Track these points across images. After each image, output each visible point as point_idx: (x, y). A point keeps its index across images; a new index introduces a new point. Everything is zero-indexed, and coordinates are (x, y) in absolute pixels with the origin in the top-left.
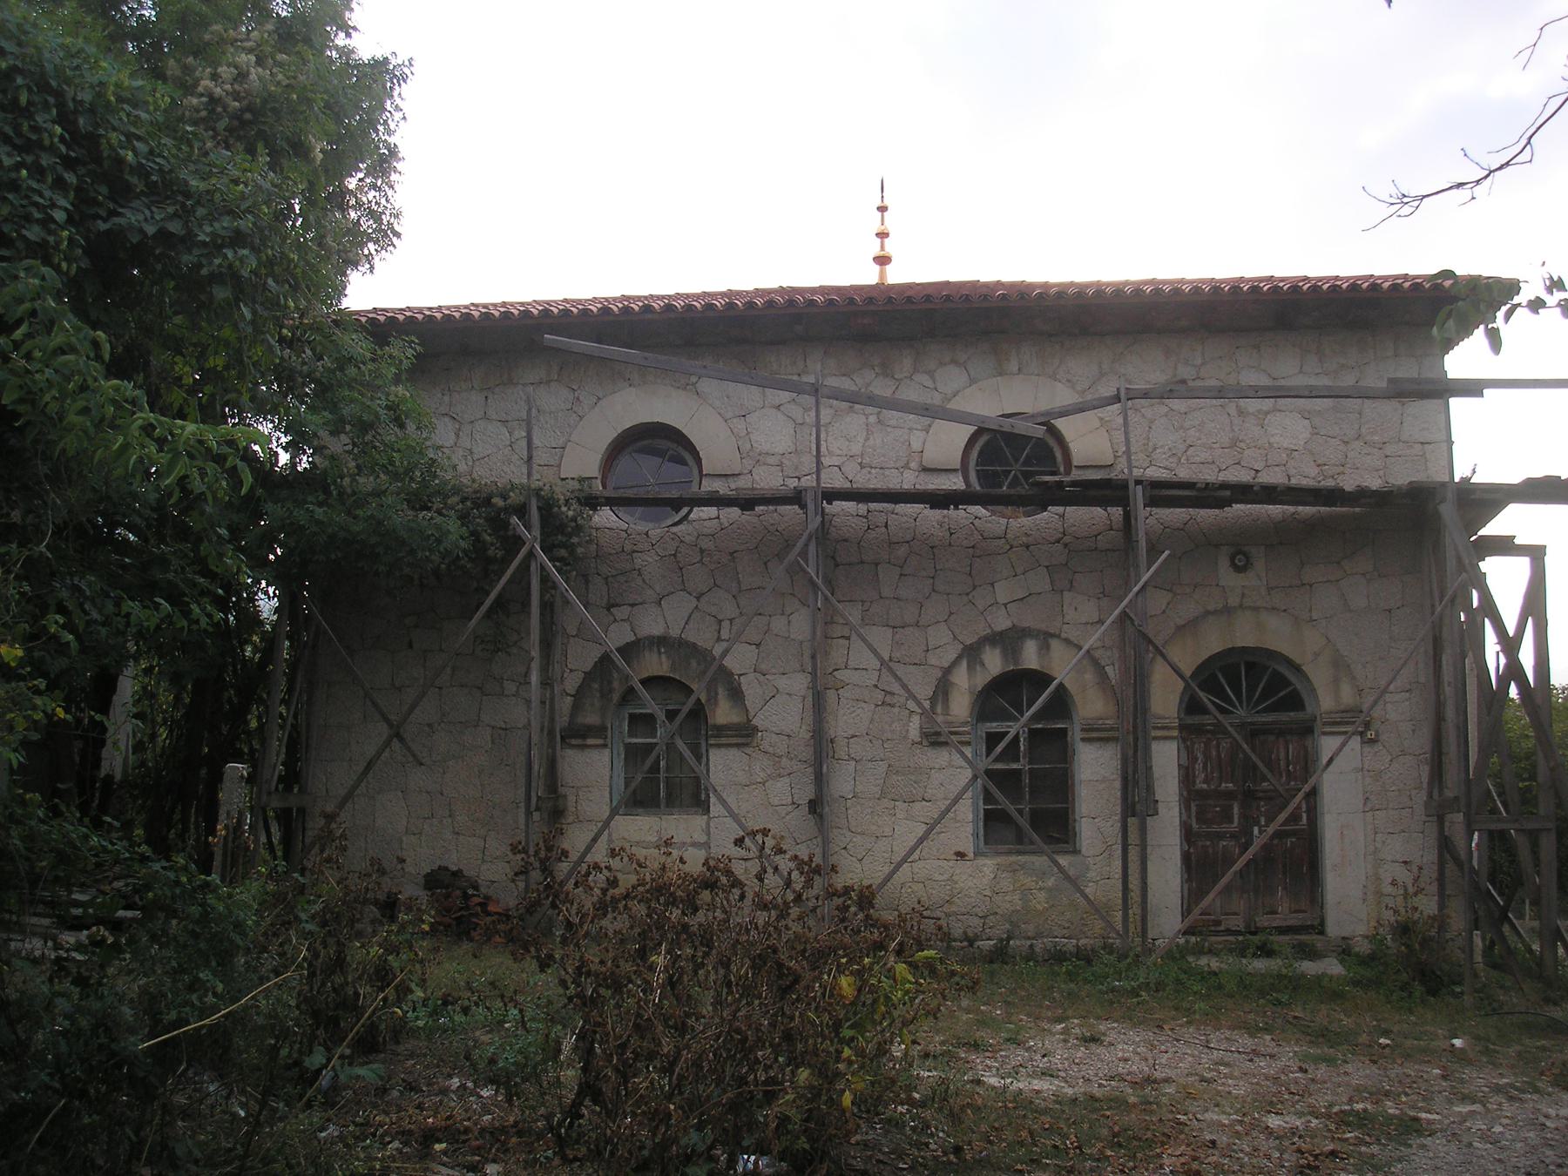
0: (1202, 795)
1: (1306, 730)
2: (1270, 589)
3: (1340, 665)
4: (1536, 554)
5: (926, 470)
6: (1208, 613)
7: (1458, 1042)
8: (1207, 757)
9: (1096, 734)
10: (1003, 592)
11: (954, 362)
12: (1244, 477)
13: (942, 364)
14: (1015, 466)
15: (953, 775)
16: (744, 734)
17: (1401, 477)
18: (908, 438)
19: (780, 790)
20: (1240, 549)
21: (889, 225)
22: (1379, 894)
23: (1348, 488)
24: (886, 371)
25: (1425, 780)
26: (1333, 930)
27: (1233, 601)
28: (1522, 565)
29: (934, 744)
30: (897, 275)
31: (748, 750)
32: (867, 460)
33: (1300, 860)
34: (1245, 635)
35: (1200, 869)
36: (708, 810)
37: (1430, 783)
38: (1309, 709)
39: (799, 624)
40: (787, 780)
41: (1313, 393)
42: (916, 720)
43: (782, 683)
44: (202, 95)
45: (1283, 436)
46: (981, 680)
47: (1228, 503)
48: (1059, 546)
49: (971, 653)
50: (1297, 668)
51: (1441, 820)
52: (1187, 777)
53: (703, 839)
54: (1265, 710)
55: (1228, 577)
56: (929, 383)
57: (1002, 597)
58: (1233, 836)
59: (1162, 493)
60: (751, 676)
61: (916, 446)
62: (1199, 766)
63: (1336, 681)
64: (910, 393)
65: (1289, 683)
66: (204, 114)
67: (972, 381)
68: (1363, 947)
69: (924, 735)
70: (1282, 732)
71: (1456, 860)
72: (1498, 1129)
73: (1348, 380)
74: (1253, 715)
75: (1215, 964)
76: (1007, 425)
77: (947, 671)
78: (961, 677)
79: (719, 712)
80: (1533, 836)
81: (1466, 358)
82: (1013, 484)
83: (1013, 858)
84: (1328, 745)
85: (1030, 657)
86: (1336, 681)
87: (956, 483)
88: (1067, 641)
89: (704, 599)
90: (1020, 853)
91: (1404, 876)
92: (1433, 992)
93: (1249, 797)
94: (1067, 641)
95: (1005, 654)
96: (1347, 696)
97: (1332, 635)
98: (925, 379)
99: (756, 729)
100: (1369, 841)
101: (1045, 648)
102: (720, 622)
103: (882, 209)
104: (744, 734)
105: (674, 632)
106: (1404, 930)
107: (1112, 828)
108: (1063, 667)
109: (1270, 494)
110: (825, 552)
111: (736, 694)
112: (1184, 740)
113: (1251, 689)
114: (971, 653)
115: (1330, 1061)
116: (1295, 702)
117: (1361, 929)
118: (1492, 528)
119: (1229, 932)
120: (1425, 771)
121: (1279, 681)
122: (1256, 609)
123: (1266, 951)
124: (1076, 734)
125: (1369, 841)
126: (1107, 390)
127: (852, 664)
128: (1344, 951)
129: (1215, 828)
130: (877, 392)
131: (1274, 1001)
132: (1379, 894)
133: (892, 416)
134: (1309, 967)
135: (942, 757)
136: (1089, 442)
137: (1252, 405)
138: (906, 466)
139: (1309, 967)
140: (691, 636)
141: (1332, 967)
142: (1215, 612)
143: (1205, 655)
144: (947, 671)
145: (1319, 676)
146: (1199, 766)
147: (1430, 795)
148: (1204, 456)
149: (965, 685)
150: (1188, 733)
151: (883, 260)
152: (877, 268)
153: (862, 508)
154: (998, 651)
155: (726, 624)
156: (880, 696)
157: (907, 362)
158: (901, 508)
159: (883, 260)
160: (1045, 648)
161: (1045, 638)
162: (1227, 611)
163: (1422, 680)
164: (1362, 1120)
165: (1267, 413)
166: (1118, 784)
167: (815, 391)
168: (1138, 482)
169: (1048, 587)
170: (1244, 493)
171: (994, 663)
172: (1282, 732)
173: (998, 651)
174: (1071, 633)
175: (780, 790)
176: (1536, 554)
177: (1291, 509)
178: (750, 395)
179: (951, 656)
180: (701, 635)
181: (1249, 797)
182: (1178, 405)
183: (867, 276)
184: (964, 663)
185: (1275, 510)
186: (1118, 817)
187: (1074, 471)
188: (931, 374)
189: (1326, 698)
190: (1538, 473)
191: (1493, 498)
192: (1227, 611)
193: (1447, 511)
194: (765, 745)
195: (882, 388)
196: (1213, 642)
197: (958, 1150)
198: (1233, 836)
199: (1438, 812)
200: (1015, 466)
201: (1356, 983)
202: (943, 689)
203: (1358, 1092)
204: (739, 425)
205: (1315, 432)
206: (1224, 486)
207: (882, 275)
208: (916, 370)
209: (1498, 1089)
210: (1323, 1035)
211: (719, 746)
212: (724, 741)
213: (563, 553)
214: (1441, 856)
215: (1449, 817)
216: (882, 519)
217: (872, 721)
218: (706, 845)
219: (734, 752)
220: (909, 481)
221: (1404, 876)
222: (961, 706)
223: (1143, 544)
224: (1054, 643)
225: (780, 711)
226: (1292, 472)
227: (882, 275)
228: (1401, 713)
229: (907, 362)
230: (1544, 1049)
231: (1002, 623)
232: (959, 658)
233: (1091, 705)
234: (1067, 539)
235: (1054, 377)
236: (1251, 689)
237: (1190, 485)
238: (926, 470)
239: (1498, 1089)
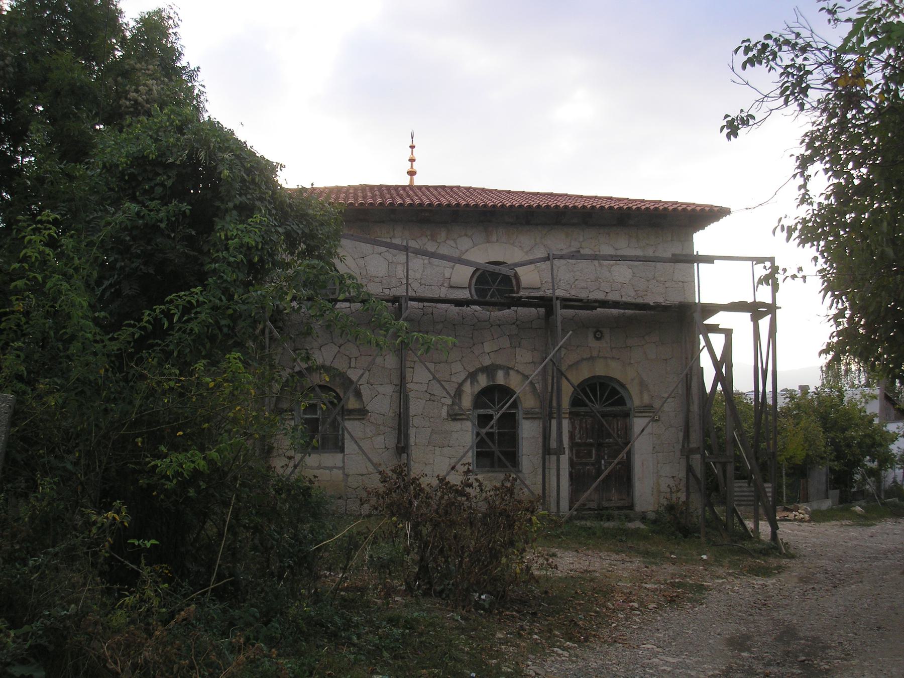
0: (578, 445)
1: (627, 415)
2: (612, 349)
3: (642, 385)
4: (728, 333)
5: (451, 287)
6: (583, 359)
7: (704, 557)
8: (581, 427)
9: (530, 415)
10: (487, 347)
11: (466, 235)
12: (600, 296)
13: (460, 236)
14: (495, 286)
15: (465, 435)
16: (362, 413)
17: (674, 298)
18: (443, 270)
19: (379, 441)
20: (598, 330)
21: (416, 155)
22: (659, 492)
23: (652, 304)
24: (433, 238)
25: (681, 439)
26: (638, 508)
27: (595, 354)
28: (723, 336)
29: (454, 420)
30: (418, 181)
31: (364, 422)
32: (423, 282)
33: (623, 477)
34: (600, 370)
35: (578, 480)
36: (342, 450)
37: (684, 439)
38: (628, 405)
39: (390, 361)
40: (382, 436)
41: (637, 259)
42: (445, 408)
43: (381, 389)
44: (130, 100)
45: (615, 275)
46: (477, 389)
47: (595, 308)
48: (514, 326)
49: (472, 376)
50: (623, 386)
51: (688, 458)
52: (572, 436)
53: (341, 465)
54: (611, 405)
55: (592, 343)
56: (454, 245)
57: (487, 350)
58: (593, 464)
59: (568, 303)
60: (366, 386)
61: (447, 275)
62: (577, 431)
63: (641, 393)
64: (444, 250)
65: (618, 393)
66: (132, 109)
67: (475, 245)
68: (652, 516)
69: (449, 415)
70: (615, 416)
71: (695, 476)
72: (736, 588)
73: (650, 252)
74: (602, 408)
75: (588, 524)
76: (491, 268)
77: (461, 385)
78: (467, 388)
79: (350, 403)
80: (724, 465)
81: (703, 241)
82: (492, 296)
83: (490, 474)
84: (638, 423)
85: (500, 379)
86: (641, 393)
87: (465, 294)
88: (518, 371)
89: (342, 347)
90: (493, 472)
91: (671, 483)
92: (685, 537)
93: (600, 446)
94: (518, 371)
95: (488, 376)
96: (646, 399)
97: (636, 369)
98: (451, 243)
99: (368, 411)
100: (654, 468)
101: (507, 374)
102: (350, 359)
103: (412, 147)
104: (362, 413)
105: (328, 363)
106: (671, 508)
107: (538, 460)
108: (514, 382)
109: (616, 305)
110: (402, 323)
111: (358, 394)
112: (570, 419)
113: (602, 395)
114: (472, 376)
115: (656, 564)
116: (621, 402)
117: (651, 508)
118: (710, 321)
119: (590, 509)
120: (681, 434)
121: (614, 392)
122: (606, 358)
123: (609, 518)
124: (520, 415)
125: (654, 468)
126: (540, 253)
127: (414, 380)
128: (643, 518)
129: (584, 460)
130: (429, 249)
131: (621, 540)
132: (659, 492)
133: (435, 261)
134: (632, 525)
135: (457, 425)
136: (531, 278)
137: (605, 262)
138: (442, 285)
139: (632, 525)
140: (335, 365)
141: (637, 525)
142: (586, 359)
143: (581, 379)
144: (461, 385)
145: (634, 390)
146: (577, 431)
147: (683, 446)
148: (583, 284)
149: (469, 392)
150: (573, 415)
151: (412, 173)
152: (409, 177)
153: (421, 305)
154: (485, 375)
155: (353, 360)
156: (428, 396)
157: (444, 234)
158: (439, 305)
159: (412, 173)
160: (507, 374)
161: (507, 369)
162: (591, 359)
163: (680, 392)
164: (680, 585)
165: (612, 266)
166: (540, 440)
167: (406, 249)
168: (557, 298)
169: (509, 345)
170: (604, 304)
171: (483, 381)
172: (615, 416)
173: (485, 375)
174: (519, 367)
175: (379, 441)
176: (728, 333)
177: (622, 311)
178: (366, 248)
179: (463, 376)
180: (340, 365)
181: (600, 446)
182: (573, 261)
183: (405, 181)
184: (469, 381)
185: (615, 311)
186: (541, 455)
187: (522, 290)
188: (454, 240)
189: (636, 400)
190: (737, 300)
191: (712, 309)
192: (591, 359)
193: (697, 316)
194: (372, 419)
195: (431, 247)
196: (584, 373)
197: (546, 592)
198: (593, 464)
199: (687, 452)
200: (495, 286)
201: (653, 532)
202: (459, 393)
203: (673, 576)
204: (361, 262)
205: (634, 275)
206: (596, 301)
207: (412, 180)
208: (447, 238)
209: (730, 574)
210: (646, 554)
211: (349, 419)
212: (352, 417)
213: (280, 324)
214: (687, 475)
215: (691, 456)
216: (430, 310)
217: (424, 408)
218: (343, 468)
219: (357, 422)
220: (443, 293)
221: (671, 483)
222: (467, 402)
223: (560, 328)
224: (512, 372)
225: (380, 401)
226: (623, 294)
227: (412, 180)
228: (671, 409)
229: (444, 234)
230: (739, 560)
231: (487, 362)
232: (466, 379)
233: (529, 402)
234: (518, 323)
235: (513, 244)
236: (602, 395)
237: (580, 300)
238: (451, 287)
239: (730, 574)
